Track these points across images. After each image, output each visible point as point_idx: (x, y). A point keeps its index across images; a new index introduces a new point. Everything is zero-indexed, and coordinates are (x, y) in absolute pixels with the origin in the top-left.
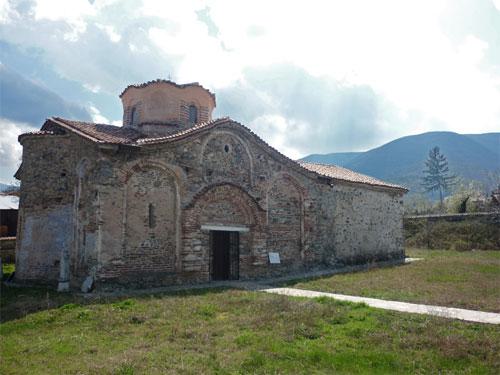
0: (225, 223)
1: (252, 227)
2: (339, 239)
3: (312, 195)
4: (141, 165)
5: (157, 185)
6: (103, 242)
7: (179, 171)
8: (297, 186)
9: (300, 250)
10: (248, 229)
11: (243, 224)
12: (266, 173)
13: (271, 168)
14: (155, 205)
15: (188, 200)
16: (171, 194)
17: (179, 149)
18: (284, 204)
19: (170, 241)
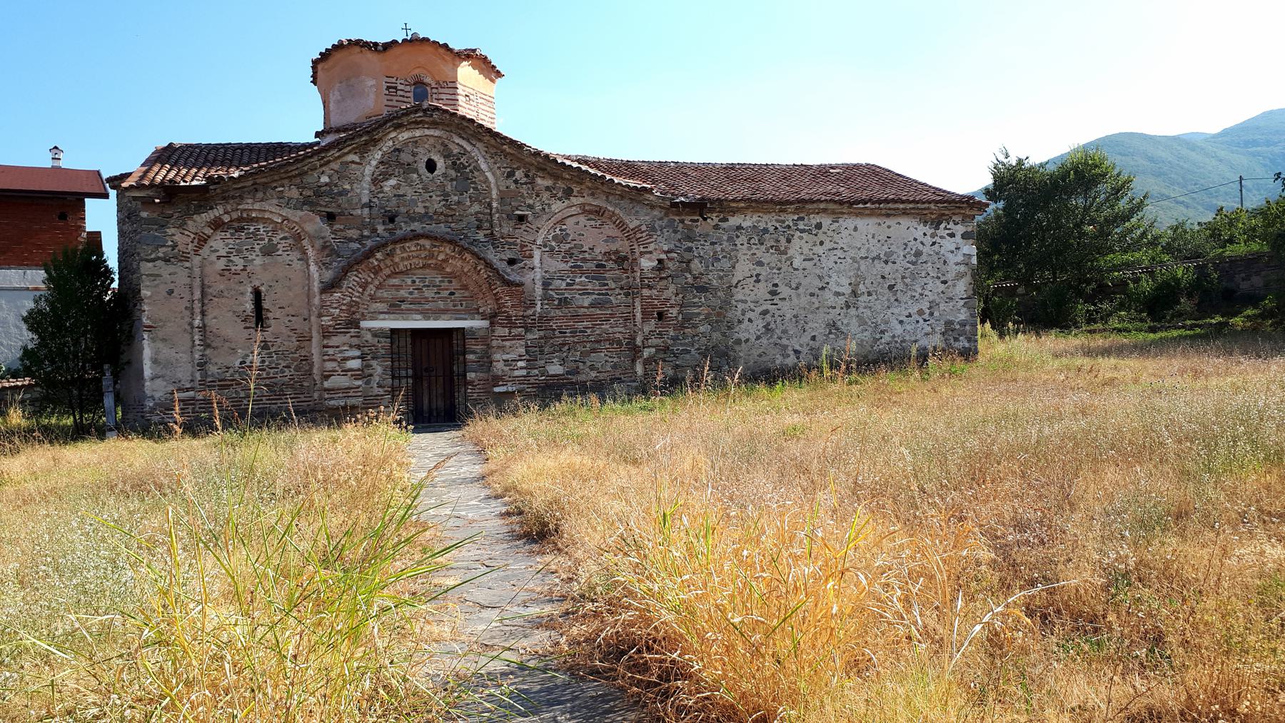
0: (426, 315)
1: (492, 317)
4: (226, 218)
5: (269, 251)
6: (155, 361)
7: (315, 224)
8: (621, 226)
9: (633, 361)
10: (485, 323)
11: (474, 312)
12: (531, 207)
13: (546, 195)
14: (263, 289)
15: (328, 275)
16: (298, 265)
18: (591, 266)
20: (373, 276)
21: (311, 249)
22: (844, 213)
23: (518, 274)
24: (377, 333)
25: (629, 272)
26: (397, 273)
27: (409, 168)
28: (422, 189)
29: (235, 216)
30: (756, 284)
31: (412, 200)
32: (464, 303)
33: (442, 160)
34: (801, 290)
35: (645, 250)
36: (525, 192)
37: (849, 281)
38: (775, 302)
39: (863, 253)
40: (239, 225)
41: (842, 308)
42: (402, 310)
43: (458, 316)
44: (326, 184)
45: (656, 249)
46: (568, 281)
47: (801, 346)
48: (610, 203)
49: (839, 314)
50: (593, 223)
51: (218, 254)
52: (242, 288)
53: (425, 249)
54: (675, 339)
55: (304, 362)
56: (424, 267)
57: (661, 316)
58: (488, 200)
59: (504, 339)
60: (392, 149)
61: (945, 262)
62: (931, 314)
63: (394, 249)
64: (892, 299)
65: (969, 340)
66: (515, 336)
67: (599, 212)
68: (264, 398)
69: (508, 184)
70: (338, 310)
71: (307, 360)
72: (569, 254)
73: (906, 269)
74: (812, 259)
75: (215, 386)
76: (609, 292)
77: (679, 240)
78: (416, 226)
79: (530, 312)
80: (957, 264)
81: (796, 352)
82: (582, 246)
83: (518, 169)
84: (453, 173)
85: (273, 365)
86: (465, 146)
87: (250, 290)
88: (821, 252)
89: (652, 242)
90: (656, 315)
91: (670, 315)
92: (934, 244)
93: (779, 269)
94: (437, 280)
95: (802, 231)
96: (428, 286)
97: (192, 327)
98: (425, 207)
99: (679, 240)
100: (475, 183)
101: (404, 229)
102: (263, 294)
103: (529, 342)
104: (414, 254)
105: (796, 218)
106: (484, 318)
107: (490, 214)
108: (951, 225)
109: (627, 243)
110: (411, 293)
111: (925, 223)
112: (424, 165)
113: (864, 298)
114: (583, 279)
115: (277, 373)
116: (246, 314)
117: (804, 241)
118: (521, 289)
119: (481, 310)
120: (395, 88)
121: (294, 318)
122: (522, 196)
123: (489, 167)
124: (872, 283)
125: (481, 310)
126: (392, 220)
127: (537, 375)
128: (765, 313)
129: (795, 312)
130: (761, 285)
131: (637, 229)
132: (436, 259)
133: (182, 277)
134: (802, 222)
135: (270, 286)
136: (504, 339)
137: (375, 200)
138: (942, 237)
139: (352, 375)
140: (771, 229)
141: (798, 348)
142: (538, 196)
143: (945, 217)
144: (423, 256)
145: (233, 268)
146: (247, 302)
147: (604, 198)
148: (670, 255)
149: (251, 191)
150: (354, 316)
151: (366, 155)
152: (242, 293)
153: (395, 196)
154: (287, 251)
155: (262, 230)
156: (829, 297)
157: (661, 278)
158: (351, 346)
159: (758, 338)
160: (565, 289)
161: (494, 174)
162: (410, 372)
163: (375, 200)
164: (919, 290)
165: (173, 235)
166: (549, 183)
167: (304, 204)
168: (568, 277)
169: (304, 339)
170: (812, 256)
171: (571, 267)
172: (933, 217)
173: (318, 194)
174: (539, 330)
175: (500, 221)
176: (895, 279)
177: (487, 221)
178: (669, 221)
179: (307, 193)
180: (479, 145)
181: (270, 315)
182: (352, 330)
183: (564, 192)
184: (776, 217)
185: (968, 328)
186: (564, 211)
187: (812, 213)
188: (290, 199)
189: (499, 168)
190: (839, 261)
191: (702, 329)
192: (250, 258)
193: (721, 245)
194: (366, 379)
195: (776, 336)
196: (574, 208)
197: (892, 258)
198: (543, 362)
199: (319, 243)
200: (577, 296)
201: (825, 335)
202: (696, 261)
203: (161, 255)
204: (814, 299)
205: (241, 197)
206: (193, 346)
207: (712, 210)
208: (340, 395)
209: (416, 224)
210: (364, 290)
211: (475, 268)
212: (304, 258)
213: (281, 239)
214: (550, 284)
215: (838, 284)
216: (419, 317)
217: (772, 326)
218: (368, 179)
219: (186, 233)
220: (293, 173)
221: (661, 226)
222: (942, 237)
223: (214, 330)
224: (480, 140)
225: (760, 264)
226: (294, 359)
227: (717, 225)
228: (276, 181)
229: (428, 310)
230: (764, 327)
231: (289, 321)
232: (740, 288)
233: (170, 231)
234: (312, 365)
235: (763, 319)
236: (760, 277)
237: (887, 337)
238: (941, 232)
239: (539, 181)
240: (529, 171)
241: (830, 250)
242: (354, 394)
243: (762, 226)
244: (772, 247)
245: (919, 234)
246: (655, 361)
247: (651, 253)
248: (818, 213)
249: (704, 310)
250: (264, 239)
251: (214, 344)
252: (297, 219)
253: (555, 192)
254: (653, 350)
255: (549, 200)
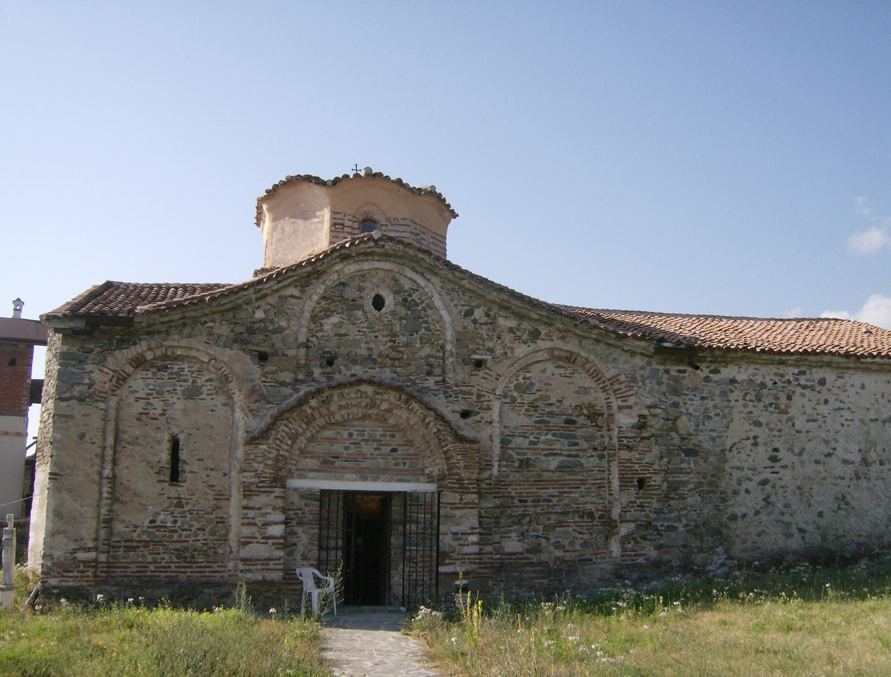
4: (149, 356)
5: (192, 393)
8: (596, 375)
10: (432, 487)
11: (418, 473)
12: (491, 351)
13: (508, 338)
14: (181, 437)
15: (257, 425)
16: (221, 411)
18: (558, 421)
19: (220, 513)
20: (305, 427)
21: (237, 393)
22: (849, 368)
23: (473, 428)
24: (306, 495)
25: (604, 430)
26: (332, 424)
27: (354, 305)
29: (159, 353)
30: (753, 448)
31: (354, 341)
32: (407, 462)
33: (391, 296)
34: (805, 457)
35: (625, 404)
37: (858, 447)
38: (776, 469)
39: (872, 415)
41: (851, 479)
42: (336, 468)
43: (400, 477)
44: (261, 321)
45: (636, 403)
46: (531, 438)
47: (806, 523)
49: (849, 486)
50: (562, 371)
51: (137, 395)
52: (159, 435)
54: (659, 512)
55: (220, 525)
56: (363, 417)
57: (641, 483)
58: (441, 342)
60: (336, 283)
63: (331, 396)
66: (468, 503)
67: (570, 359)
68: (173, 565)
69: (465, 324)
70: (262, 465)
71: (224, 522)
72: (533, 406)
75: (119, 547)
78: (358, 370)
79: (486, 475)
83: (478, 307)
84: (402, 311)
85: (186, 527)
86: (418, 281)
87: (167, 437)
89: (632, 395)
90: (636, 483)
91: (653, 483)
93: (780, 431)
95: (804, 387)
96: (367, 441)
97: (101, 478)
98: (369, 349)
99: (664, 394)
100: (427, 322)
101: (343, 373)
102: (181, 443)
103: (483, 512)
104: (353, 402)
105: (796, 372)
106: (430, 479)
107: (443, 358)
109: (602, 396)
110: (346, 448)
112: (370, 301)
113: (875, 468)
114: (549, 437)
115: (189, 536)
116: (161, 465)
117: (806, 399)
118: (476, 446)
119: (427, 471)
122: (482, 338)
123: (445, 304)
124: (884, 450)
125: (427, 471)
126: (330, 363)
127: (491, 553)
128: (764, 483)
129: (799, 483)
130: (761, 448)
131: (614, 380)
134: (803, 377)
135: (190, 435)
137: (314, 339)
140: (770, 384)
142: (499, 338)
144: (363, 404)
145: (152, 412)
147: (577, 342)
148: (653, 411)
150: (280, 473)
151: (307, 289)
153: (336, 335)
154: (211, 394)
155: (186, 370)
157: (643, 438)
158: (274, 508)
159: (757, 513)
160: (528, 449)
161: (449, 312)
162: (340, 542)
163: (314, 339)
165: (92, 372)
166: (512, 323)
169: (222, 497)
170: (815, 417)
171: (536, 422)
173: (251, 331)
175: (454, 366)
177: (439, 366)
178: (652, 370)
180: (434, 279)
181: (187, 468)
182: (277, 489)
183: (531, 333)
184: (775, 370)
187: (815, 367)
188: (219, 336)
189: (456, 306)
190: (846, 423)
191: (690, 500)
192: (170, 401)
193: (712, 400)
194: (288, 549)
195: (777, 511)
196: (541, 353)
198: (498, 536)
199: (248, 386)
200: (543, 458)
201: (833, 511)
202: (684, 418)
203: (76, 394)
204: (820, 468)
205: (168, 333)
206: (100, 499)
208: (259, 567)
209: (358, 367)
210: (293, 443)
211: (424, 420)
212: (229, 404)
213: (207, 381)
214: (510, 442)
216: (354, 476)
218: (307, 315)
219: (105, 370)
220: (226, 307)
221: (642, 376)
223: (125, 482)
224: (436, 274)
225: (758, 424)
226: (209, 521)
227: (708, 377)
228: (206, 315)
229: (365, 468)
230: (764, 500)
231: (208, 476)
232: (735, 452)
233: (89, 367)
234: (228, 530)
235: (763, 490)
236: (759, 440)
239: (501, 321)
240: (490, 309)
241: (836, 410)
242: (273, 567)
243: (759, 379)
244: (771, 404)
247: (630, 407)
248: (821, 367)
249: (693, 478)
251: (123, 499)
252: (226, 359)
253: (519, 334)
254: (632, 526)
255: (513, 343)
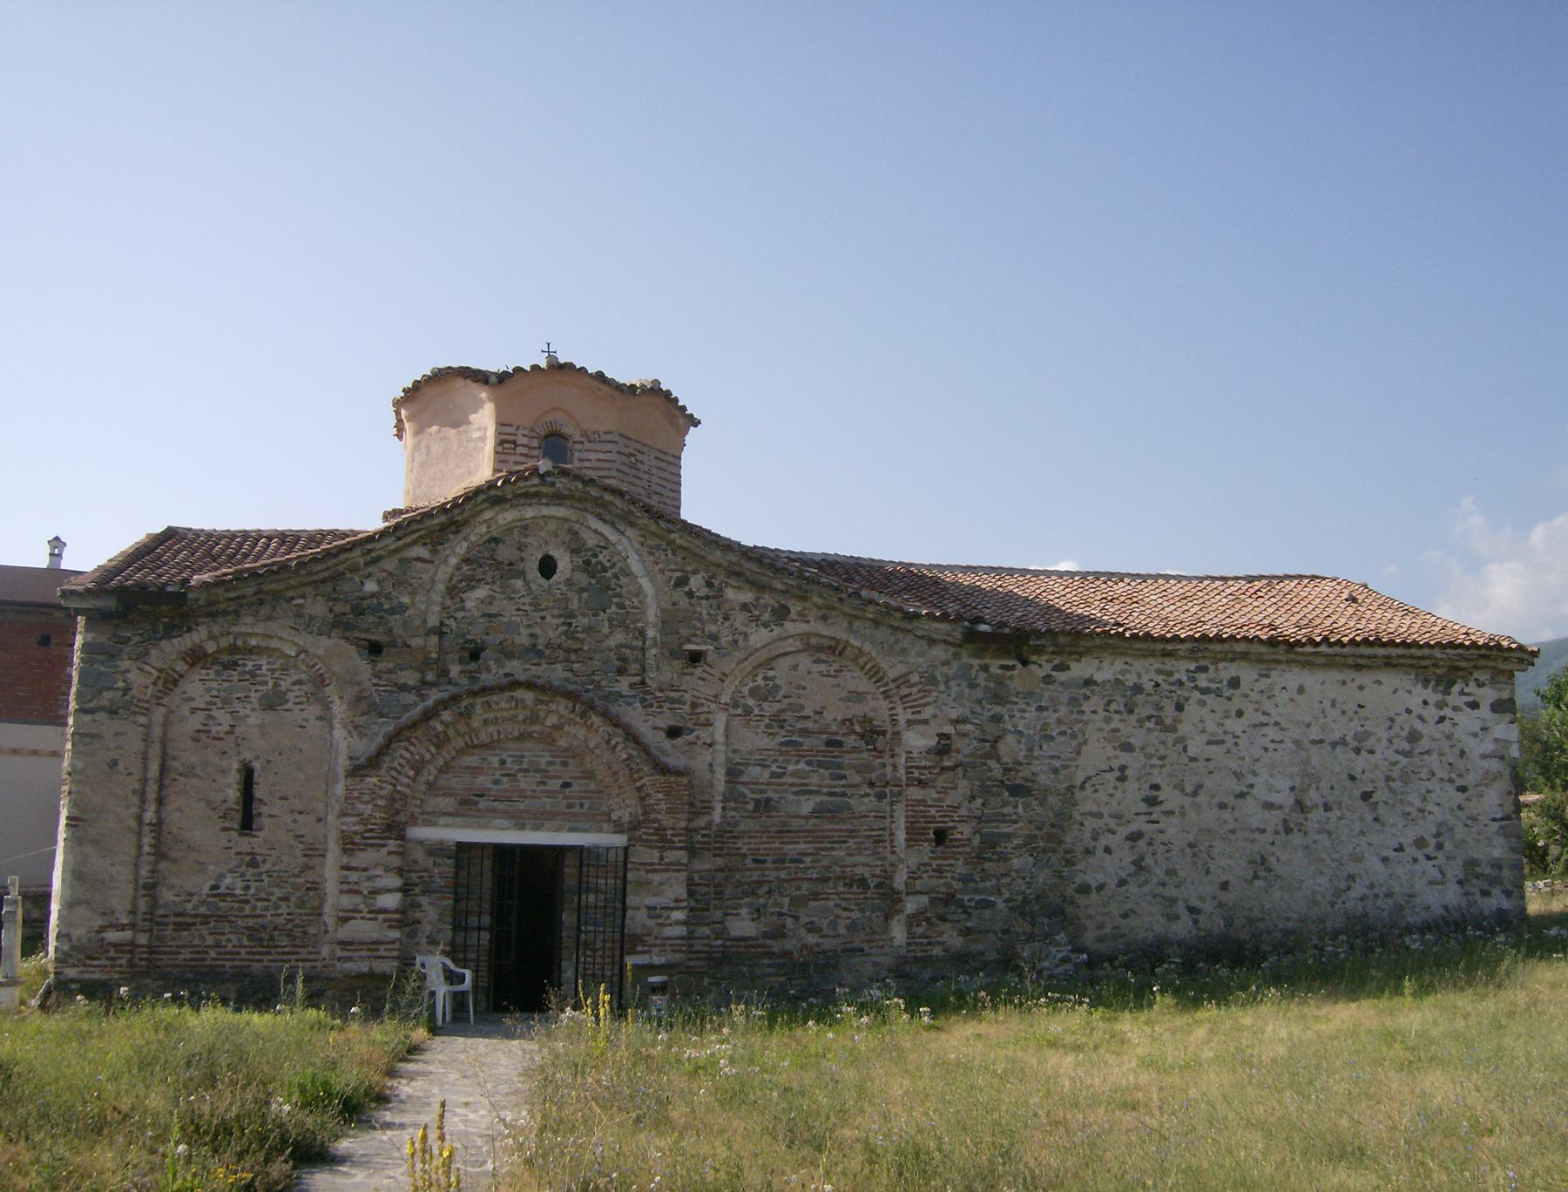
2: (1105, 868)
3: (946, 708)
4: (211, 647)
5: (273, 702)
8: (875, 674)
10: (620, 840)
12: (714, 637)
13: (740, 618)
14: (257, 765)
16: (315, 727)
17: (345, 587)
19: (311, 876)
20: (433, 750)
21: (338, 702)
22: (1278, 662)
23: (684, 753)
24: (436, 850)
25: (887, 756)
26: (475, 747)
27: (511, 570)
28: (531, 605)
29: (225, 642)
32: (586, 802)
33: (567, 558)
34: (1202, 798)
35: (917, 717)
36: (704, 613)
37: (1290, 783)
38: (1154, 817)
39: (1315, 733)
40: (230, 659)
41: (1277, 833)
43: (575, 825)
44: (373, 595)
45: (935, 716)
46: (774, 768)
47: (1201, 898)
48: (856, 632)
49: (1273, 843)
50: (823, 667)
52: (225, 763)
53: (524, 707)
54: (965, 879)
55: (311, 893)
56: (522, 737)
57: (941, 837)
59: (650, 868)
60: (485, 538)
61: (1463, 753)
62: (1439, 847)
63: (473, 705)
64: (1369, 818)
65: (1508, 894)
67: (835, 649)
68: (243, 951)
69: (675, 598)
70: (370, 807)
72: (778, 720)
73: (1395, 764)
74: (1222, 742)
76: (849, 791)
77: (979, 702)
78: (514, 666)
79: (702, 822)
80: (1484, 756)
81: (1192, 910)
82: (802, 707)
83: (695, 572)
84: (583, 579)
85: (263, 895)
86: (606, 534)
87: (236, 766)
88: (1238, 731)
89: (928, 704)
90: (932, 836)
92: (1442, 719)
93: (1162, 758)
94: (543, 760)
98: (532, 635)
100: (619, 596)
101: (494, 671)
103: (696, 876)
104: (506, 714)
106: (618, 828)
108: (1472, 688)
110: (496, 782)
111: (1426, 683)
113: (1317, 815)
114: (802, 766)
115: (266, 909)
116: (227, 805)
119: (614, 816)
120: (514, 443)
121: (302, 817)
122: (700, 619)
124: (1332, 788)
126: (475, 656)
127: (708, 937)
128: (1135, 837)
129: (1191, 837)
130: (1131, 786)
131: (903, 680)
132: (543, 724)
133: (134, 741)
134: (1203, 676)
136: (650, 868)
137: (451, 622)
138: (1456, 709)
139: (385, 920)
140: (1148, 686)
141: (1195, 902)
142: (726, 618)
143: (1460, 673)
145: (214, 729)
146: (229, 786)
147: (845, 624)
148: (960, 727)
149: (253, 604)
152: (224, 772)
155: (264, 668)
156: (1251, 811)
159: (1122, 883)
160: (768, 784)
164: (1418, 802)
165: (128, 671)
166: (747, 596)
167: (335, 625)
168: (775, 761)
169: (315, 852)
171: (782, 744)
172: (1439, 671)
173: (359, 611)
174: (715, 856)
176: (1373, 781)
177: (636, 660)
179: (339, 608)
180: (630, 532)
181: (264, 809)
183: (774, 612)
184: (1157, 666)
185: (1506, 873)
186: (773, 646)
187: (1222, 660)
188: (312, 618)
189: (662, 571)
190: (1271, 746)
191: (1016, 862)
194: (408, 929)
195: (1155, 881)
196: (790, 641)
197: (1369, 744)
200: (791, 797)
202: (1010, 739)
204: (1226, 815)
205: (237, 614)
207: (1039, 650)
208: (364, 953)
210: (417, 774)
211: (608, 742)
212: (326, 718)
213: (294, 684)
214: (741, 773)
215: (1270, 788)
217: (1148, 861)
218: (441, 587)
219: (148, 668)
220: (321, 576)
221: (946, 676)
222: (1456, 709)
223: (175, 830)
224: (632, 524)
225: (1127, 747)
226: (295, 887)
230: (1134, 863)
231: (295, 821)
232: (1089, 790)
233: (124, 664)
235: (1134, 847)
237: (1358, 890)
238: (1454, 698)
239: (730, 594)
240: (714, 576)
241: (1255, 726)
243: (1131, 680)
244: (1149, 718)
245: (1415, 702)
246: (928, 920)
247: (926, 722)
248: (1232, 660)
249: (1022, 829)
250: (266, 683)
251: (173, 854)
252: (321, 652)
253: (757, 613)
254: (924, 899)
